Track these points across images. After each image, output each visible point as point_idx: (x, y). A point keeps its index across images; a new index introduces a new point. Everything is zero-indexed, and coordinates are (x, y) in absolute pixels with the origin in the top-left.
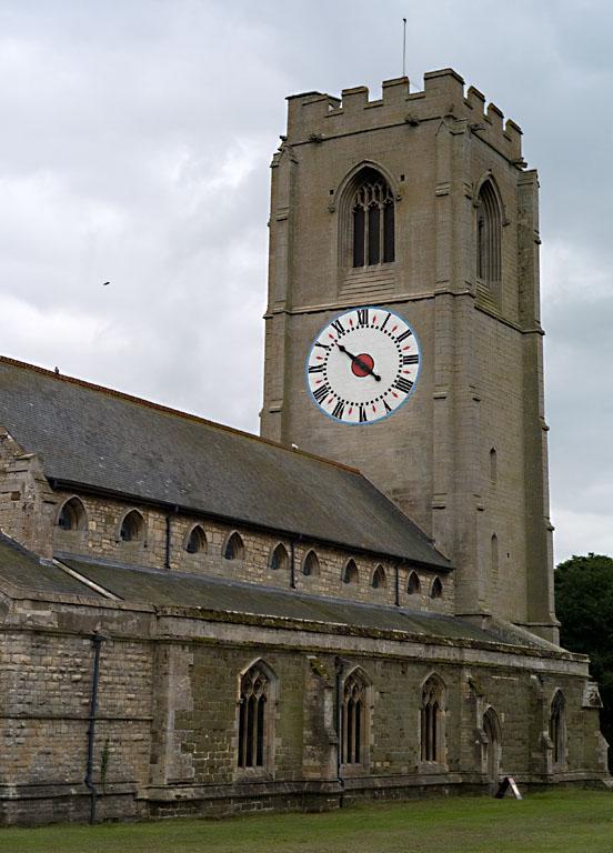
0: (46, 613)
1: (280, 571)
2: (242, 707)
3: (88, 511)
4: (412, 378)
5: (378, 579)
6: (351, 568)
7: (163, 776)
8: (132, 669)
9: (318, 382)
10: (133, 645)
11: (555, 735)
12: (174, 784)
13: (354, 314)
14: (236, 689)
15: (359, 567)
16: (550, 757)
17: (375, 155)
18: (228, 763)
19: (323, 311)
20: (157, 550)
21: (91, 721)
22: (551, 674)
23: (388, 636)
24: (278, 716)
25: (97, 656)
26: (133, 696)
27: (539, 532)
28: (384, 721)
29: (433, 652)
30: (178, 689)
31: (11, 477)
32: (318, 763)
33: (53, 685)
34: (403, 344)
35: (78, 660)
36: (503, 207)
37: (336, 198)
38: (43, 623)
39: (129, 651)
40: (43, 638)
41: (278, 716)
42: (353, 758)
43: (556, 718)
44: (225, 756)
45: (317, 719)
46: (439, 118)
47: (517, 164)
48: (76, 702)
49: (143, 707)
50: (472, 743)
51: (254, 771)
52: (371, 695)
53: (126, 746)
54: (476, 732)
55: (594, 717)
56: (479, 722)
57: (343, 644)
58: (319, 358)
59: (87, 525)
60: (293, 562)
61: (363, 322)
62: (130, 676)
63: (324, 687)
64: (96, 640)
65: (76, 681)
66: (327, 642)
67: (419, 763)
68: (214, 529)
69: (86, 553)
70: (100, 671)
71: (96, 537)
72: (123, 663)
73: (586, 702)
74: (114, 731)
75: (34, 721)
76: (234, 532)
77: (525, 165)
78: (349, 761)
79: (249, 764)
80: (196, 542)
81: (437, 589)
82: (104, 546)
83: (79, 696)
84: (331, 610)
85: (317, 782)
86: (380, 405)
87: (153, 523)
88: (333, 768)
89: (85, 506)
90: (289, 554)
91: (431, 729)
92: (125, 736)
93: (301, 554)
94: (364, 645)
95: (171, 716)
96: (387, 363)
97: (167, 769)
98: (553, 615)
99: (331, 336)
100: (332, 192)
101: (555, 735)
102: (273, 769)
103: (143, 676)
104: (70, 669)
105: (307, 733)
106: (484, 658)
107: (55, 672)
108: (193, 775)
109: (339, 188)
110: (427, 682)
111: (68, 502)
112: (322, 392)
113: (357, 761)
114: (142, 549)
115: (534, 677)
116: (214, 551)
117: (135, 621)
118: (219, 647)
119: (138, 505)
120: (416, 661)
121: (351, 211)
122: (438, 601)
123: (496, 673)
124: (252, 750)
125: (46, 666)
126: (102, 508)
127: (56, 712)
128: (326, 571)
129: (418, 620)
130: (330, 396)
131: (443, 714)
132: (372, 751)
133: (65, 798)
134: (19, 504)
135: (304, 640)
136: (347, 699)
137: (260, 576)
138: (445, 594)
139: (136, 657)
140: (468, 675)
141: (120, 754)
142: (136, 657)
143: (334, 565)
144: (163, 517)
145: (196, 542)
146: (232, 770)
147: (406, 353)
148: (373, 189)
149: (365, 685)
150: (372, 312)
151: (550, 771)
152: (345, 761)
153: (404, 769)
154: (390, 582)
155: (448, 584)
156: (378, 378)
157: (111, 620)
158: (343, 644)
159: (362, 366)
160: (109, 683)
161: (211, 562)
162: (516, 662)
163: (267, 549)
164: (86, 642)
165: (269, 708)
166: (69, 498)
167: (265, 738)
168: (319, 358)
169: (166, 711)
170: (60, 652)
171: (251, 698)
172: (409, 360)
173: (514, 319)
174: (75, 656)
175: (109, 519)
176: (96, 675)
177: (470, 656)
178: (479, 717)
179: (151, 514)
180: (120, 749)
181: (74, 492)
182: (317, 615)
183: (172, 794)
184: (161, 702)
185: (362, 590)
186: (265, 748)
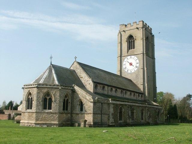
4: (138, 66)
5: (134, 95)
6: (131, 94)
11: (158, 117)
13: (129, 57)
21: (101, 114)
22: (157, 108)
23: (137, 103)
30: (112, 110)
34: (136, 61)
43: (158, 114)
47: (151, 34)
51: (121, 121)
52: (135, 111)
57: (131, 104)
61: (131, 58)
72: (105, 106)
86: (133, 70)
87: (106, 87)
93: (124, 91)
94: (134, 104)
96: (134, 64)
101: (158, 117)
112: (125, 68)
120: (141, 106)
131: (144, 114)
135: (127, 103)
143: (129, 93)
150: (132, 56)
155: (143, 95)
156: (133, 66)
158: (131, 104)
159: (131, 64)
172: (137, 63)
175: (101, 87)
178: (149, 114)
182: (128, 100)
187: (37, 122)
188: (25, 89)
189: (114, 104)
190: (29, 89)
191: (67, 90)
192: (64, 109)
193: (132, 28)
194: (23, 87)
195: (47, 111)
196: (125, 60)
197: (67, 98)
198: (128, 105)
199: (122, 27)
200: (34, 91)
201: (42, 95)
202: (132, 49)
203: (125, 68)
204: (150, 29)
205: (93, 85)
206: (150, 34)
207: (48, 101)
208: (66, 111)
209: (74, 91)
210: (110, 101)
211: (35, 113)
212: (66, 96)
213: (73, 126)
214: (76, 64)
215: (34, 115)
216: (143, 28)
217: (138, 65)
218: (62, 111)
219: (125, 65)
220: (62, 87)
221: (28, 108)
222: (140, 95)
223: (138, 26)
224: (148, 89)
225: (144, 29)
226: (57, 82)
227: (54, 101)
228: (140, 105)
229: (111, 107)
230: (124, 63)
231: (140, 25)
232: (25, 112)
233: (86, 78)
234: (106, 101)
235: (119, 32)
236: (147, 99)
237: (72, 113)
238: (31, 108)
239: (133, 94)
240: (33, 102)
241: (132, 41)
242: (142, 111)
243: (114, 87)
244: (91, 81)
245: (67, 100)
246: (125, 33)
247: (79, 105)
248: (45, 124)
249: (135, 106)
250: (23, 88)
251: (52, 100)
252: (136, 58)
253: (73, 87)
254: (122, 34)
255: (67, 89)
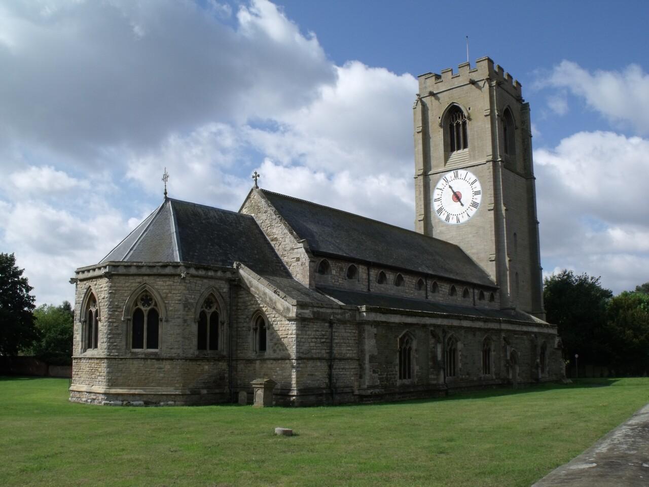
0: (307, 311)
1: (421, 292)
2: (400, 353)
3: (331, 266)
5: (465, 294)
7: (365, 384)
8: (348, 336)
9: (439, 206)
10: (348, 325)
12: (369, 387)
13: (452, 174)
14: (397, 344)
15: (456, 289)
16: (540, 371)
17: (457, 99)
18: (395, 378)
19: (439, 173)
20: (364, 283)
22: (540, 333)
23: (466, 318)
24: (417, 356)
25: (332, 330)
26: (350, 348)
27: (536, 270)
28: (466, 357)
29: (487, 325)
30: (370, 345)
31: (296, 250)
32: (435, 377)
33: (312, 344)
34: (474, 186)
35: (323, 333)
36: (515, 121)
37: (441, 120)
38: (306, 316)
39: (347, 328)
40: (306, 323)
41: (417, 356)
42: (452, 374)
43: (543, 353)
44: (393, 374)
45: (434, 357)
46: (484, 80)
47: (519, 99)
48: (323, 351)
49: (355, 353)
50: (505, 366)
51: (407, 382)
52: (460, 346)
53: (348, 371)
54: (507, 361)
55: (560, 352)
56: (508, 356)
57: (445, 322)
58: (438, 195)
59: (331, 272)
60: (426, 286)
61: (456, 176)
62: (348, 339)
63: (438, 341)
64: (331, 324)
65: (323, 342)
66: (439, 322)
67: (482, 376)
68: (390, 273)
69: (332, 285)
70: (334, 337)
71: (336, 278)
72: (344, 334)
73: (556, 346)
74: (341, 365)
75: (305, 361)
76: (399, 273)
77: (524, 101)
78: (450, 375)
79: (405, 378)
80: (382, 279)
81: (492, 298)
82: (340, 282)
83: (324, 349)
84: (415, 303)
85: (435, 385)
86: (465, 215)
87: (362, 270)
88: (442, 379)
89: (330, 263)
90: (425, 283)
91: (452, 354)
92: (347, 367)
93: (430, 283)
94: (456, 323)
95: (367, 357)
96: (467, 198)
97: (367, 381)
98: (543, 308)
99: (443, 184)
100: (440, 118)
102: (416, 380)
103: (354, 340)
104: (320, 337)
105: (430, 363)
106: (510, 327)
107: (313, 338)
108: (379, 383)
109: (443, 115)
110: (485, 339)
111: (322, 262)
112: (440, 210)
113: (454, 375)
114: (357, 282)
115: (533, 335)
116: (390, 282)
117: (349, 314)
118: (387, 324)
119: (354, 262)
120: (480, 329)
121: (449, 126)
122: (493, 303)
123: (516, 334)
124: (405, 371)
125: (309, 335)
126: (337, 264)
127: (314, 356)
128: (442, 291)
129: (483, 311)
130: (444, 212)
131: (493, 353)
132: (460, 370)
133: (321, 395)
134: (300, 263)
136: (449, 348)
137: (412, 294)
138: (496, 300)
139: (350, 331)
140: (503, 335)
141: (345, 375)
142: (350, 331)
143: (445, 288)
144: (366, 268)
145: (382, 279)
146: (396, 381)
147: (475, 190)
148: (457, 115)
149: (457, 341)
150: (460, 172)
151: (540, 377)
152: (449, 375)
153: (475, 379)
154: (471, 295)
155: (497, 295)
156: (462, 205)
157: (337, 314)
158: (445, 322)
159: (457, 197)
160: (338, 343)
161: (389, 288)
162: (525, 329)
163: (414, 281)
164: (327, 324)
165: (413, 354)
166: (322, 260)
167: (412, 366)
168: (438, 195)
169: (365, 355)
170: (315, 329)
171: (404, 348)
172: (477, 193)
173: (522, 172)
174: (322, 331)
175: (341, 269)
176: (332, 339)
177: (504, 326)
178: (508, 354)
179: (360, 266)
180: (345, 373)
181: (324, 257)
182: (434, 309)
183: (369, 392)
184: (362, 351)
185: (459, 299)
186: (411, 371)
187: (113, 391)
188: (79, 282)
189: (376, 324)
190: (88, 284)
191: (212, 283)
192: (201, 346)
193: (457, 82)
194: (74, 276)
195: (146, 350)
196: (439, 185)
197: (213, 309)
198: (435, 326)
199: (425, 83)
200: (102, 289)
201: (126, 300)
202: (459, 149)
203: (440, 210)
204: (514, 84)
205: (307, 264)
206: (514, 101)
207: (146, 319)
208: (209, 352)
209: (238, 285)
210: (365, 314)
211: (106, 361)
212: (209, 302)
213: (264, 404)
214: (256, 196)
215: (103, 368)
216: (489, 80)
217: (478, 199)
218: (192, 349)
219: (439, 199)
220: (193, 271)
221: (90, 347)
222: (487, 294)
223: (475, 77)
224: (515, 276)
225: (494, 83)
226: (178, 259)
227: (164, 319)
228: (479, 325)
229: (366, 335)
230: (436, 194)
231: (482, 72)
232: (80, 358)
233: (287, 240)
234: (347, 316)
235: (417, 98)
236: (509, 305)
237: (231, 359)
238: (96, 347)
239: (460, 290)
240: (100, 324)
241: (458, 124)
242: (487, 342)
243: (393, 269)
244: (303, 250)
245: (215, 316)
246: (438, 99)
247: (255, 330)
248: (138, 398)
249: (461, 327)
250: (73, 281)
251: (158, 315)
252: (473, 178)
253: (235, 272)
254: (429, 105)
255: (211, 278)
